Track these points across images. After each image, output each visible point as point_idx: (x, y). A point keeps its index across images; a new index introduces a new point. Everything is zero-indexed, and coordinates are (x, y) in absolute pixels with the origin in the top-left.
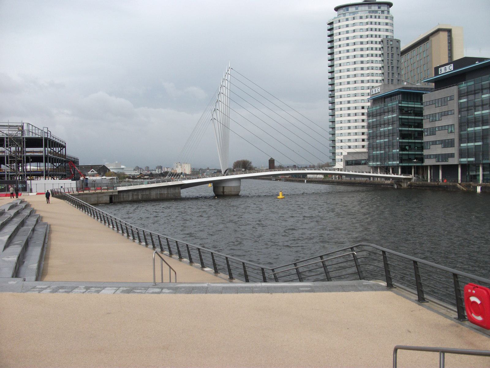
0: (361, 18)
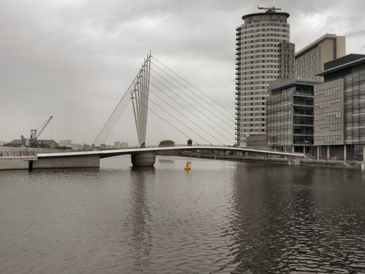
0: (264, 25)
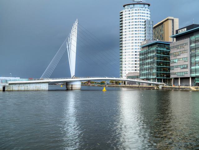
0: (136, 10)
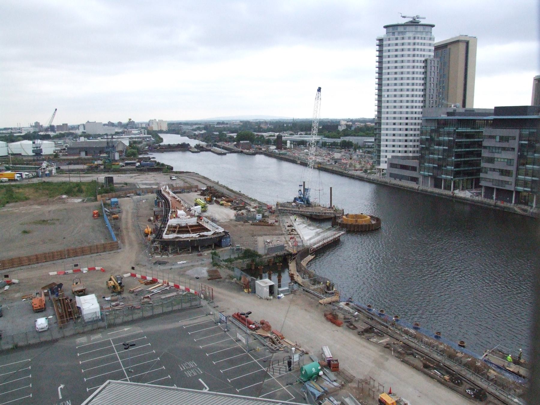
0: (409, 38)
